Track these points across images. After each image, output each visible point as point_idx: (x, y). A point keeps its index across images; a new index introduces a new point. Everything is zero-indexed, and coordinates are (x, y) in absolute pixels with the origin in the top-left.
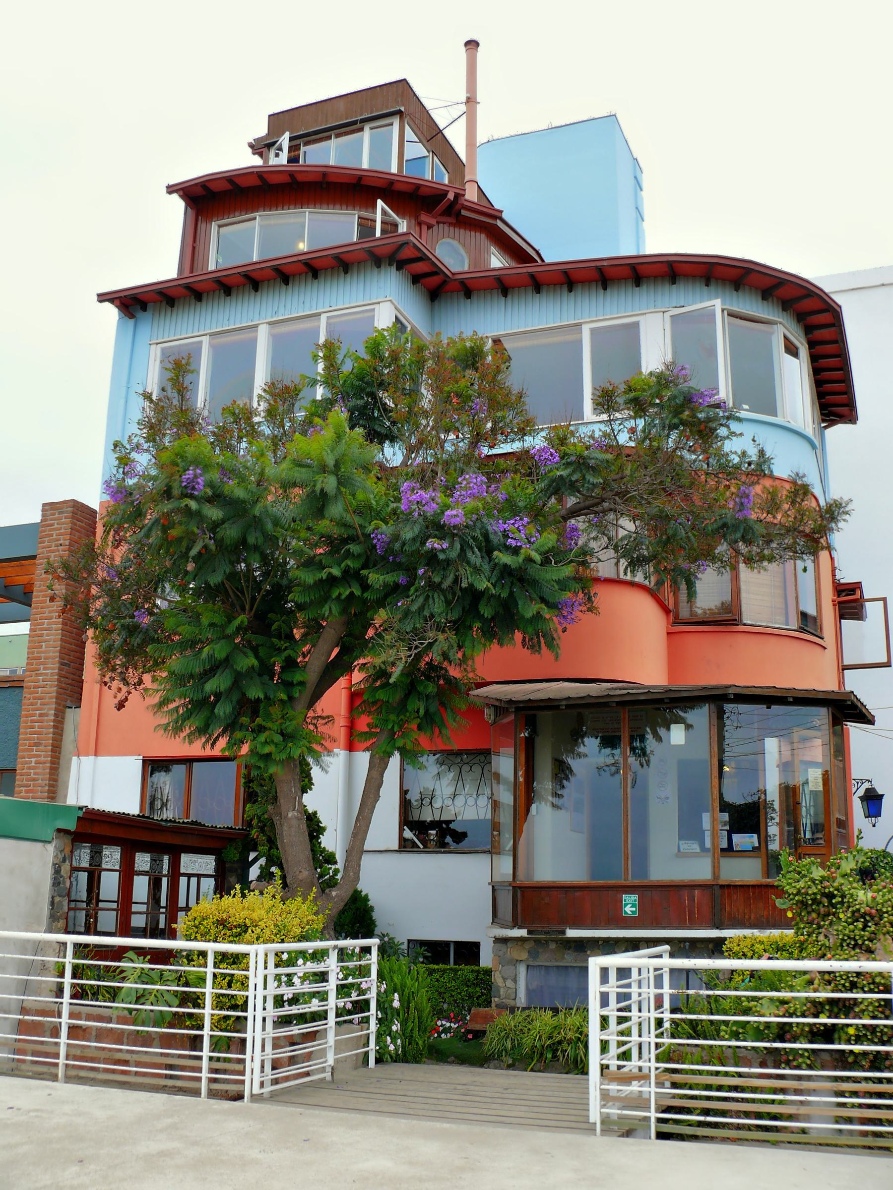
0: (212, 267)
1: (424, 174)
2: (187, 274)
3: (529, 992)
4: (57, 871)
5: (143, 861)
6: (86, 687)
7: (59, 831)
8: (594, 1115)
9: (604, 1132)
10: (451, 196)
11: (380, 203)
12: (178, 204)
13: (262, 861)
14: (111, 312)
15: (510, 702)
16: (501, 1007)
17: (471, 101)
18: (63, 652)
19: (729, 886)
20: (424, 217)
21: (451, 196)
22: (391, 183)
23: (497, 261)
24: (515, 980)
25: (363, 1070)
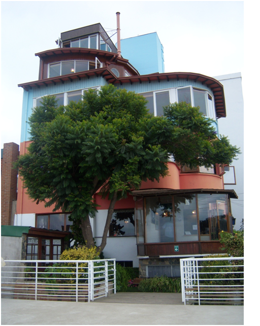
0: (48, 77)
1: (105, 49)
2: (41, 79)
3: (149, 273)
4: (23, 245)
5: (48, 242)
6: (18, 194)
7: (23, 233)
8: (184, 300)
9: (186, 304)
10: (115, 56)
11: (96, 58)
12: (38, 58)
13: (74, 241)
14: (22, 89)
15: (142, 195)
16: (142, 277)
17: (118, 29)
18: (11, 185)
19: (203, 242)
20: (107, 62)
21: (115, 56)
22: (105, 54)
23: (127, 75)
24: (145, 270)
25: (113, 294)
